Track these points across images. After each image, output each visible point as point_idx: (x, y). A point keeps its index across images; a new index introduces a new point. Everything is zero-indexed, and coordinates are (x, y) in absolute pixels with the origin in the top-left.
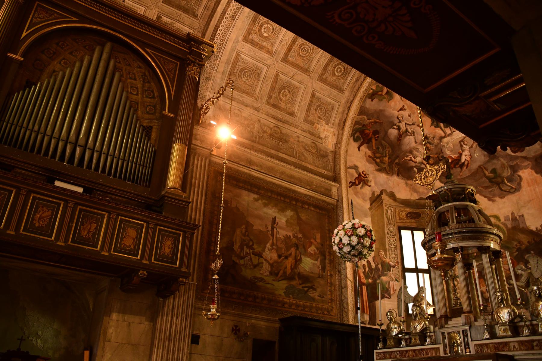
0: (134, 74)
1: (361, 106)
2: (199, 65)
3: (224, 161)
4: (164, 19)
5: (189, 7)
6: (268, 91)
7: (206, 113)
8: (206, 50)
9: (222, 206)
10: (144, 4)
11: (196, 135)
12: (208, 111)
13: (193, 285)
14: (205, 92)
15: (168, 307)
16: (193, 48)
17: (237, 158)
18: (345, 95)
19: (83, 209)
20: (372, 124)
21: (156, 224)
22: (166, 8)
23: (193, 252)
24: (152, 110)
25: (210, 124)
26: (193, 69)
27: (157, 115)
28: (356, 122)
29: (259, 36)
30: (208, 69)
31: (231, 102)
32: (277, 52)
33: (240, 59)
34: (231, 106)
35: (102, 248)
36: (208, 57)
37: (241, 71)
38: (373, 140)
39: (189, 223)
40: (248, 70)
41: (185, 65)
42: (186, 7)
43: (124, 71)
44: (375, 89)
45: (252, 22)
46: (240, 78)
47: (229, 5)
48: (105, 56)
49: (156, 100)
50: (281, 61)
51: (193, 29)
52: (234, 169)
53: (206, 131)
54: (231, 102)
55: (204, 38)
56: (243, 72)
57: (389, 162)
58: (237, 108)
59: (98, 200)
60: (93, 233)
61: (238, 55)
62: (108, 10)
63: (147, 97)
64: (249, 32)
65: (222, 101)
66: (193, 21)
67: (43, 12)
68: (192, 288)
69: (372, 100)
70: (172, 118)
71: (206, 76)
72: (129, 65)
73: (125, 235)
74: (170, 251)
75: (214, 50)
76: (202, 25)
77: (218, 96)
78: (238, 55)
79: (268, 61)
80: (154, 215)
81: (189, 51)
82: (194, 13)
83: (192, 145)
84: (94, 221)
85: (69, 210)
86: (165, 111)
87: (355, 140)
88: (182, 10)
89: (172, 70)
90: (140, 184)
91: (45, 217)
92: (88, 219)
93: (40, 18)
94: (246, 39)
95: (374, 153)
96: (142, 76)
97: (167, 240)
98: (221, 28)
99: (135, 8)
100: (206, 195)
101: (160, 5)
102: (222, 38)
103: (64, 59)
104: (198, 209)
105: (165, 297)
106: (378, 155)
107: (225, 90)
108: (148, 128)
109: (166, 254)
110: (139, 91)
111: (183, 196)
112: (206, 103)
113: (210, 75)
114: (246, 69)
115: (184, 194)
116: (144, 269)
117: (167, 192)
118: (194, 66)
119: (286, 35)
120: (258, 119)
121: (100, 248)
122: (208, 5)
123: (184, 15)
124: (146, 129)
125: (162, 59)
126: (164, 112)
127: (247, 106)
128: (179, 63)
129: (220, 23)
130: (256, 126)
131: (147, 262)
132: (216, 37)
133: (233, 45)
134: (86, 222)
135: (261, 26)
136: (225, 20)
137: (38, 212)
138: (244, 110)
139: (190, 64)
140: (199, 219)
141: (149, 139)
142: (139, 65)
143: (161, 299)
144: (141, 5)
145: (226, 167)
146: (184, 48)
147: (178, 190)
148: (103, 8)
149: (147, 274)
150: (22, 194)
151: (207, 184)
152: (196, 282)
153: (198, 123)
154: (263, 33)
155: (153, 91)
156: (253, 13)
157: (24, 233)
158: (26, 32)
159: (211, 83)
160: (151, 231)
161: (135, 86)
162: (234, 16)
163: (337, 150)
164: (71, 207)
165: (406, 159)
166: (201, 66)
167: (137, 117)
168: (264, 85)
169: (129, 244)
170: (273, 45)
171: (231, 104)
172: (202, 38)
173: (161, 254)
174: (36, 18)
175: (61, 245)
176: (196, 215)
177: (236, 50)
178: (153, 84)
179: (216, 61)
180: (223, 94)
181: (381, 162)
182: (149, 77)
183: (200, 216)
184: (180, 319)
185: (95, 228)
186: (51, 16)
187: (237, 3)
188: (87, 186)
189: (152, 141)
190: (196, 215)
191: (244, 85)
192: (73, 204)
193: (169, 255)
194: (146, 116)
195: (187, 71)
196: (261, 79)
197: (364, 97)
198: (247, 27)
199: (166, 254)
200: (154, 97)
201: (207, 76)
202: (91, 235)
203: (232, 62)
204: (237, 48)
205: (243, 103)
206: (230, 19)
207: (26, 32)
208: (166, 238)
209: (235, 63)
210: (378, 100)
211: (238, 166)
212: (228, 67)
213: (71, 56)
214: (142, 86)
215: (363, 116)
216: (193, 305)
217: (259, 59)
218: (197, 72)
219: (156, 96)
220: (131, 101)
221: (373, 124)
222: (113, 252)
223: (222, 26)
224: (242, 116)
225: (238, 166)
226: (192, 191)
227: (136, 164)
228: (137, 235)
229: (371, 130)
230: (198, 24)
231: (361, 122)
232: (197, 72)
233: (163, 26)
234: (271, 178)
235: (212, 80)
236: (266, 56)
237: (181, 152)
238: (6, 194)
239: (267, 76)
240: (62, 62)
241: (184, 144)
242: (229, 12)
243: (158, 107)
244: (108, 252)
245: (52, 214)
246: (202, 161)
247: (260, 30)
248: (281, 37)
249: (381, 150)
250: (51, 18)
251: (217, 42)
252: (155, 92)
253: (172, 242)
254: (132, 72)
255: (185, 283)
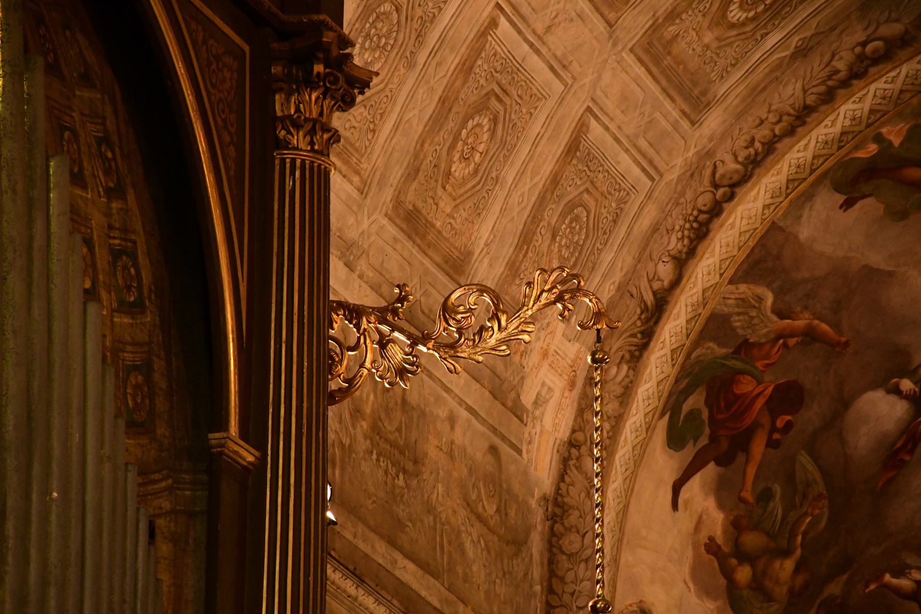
1: (774, 228)
18: (697, 134)
20: (785, 345)
28: (713, 317)
38: (758, 447)
44: (896, 142)
57: (791, 591)
69: (848, 204)
86: (225, 427)
87: (675, 440)
95: (736, 526)
106: (752, 540)
163: (575, 495)
165: (887, 586)
181: (758, 585)
197: (812, 171)
210: (881, 207)
215: (761, 290)
221: (792, 342)
229: (767, 378)
231: (737, 322)
249: (777, 507)
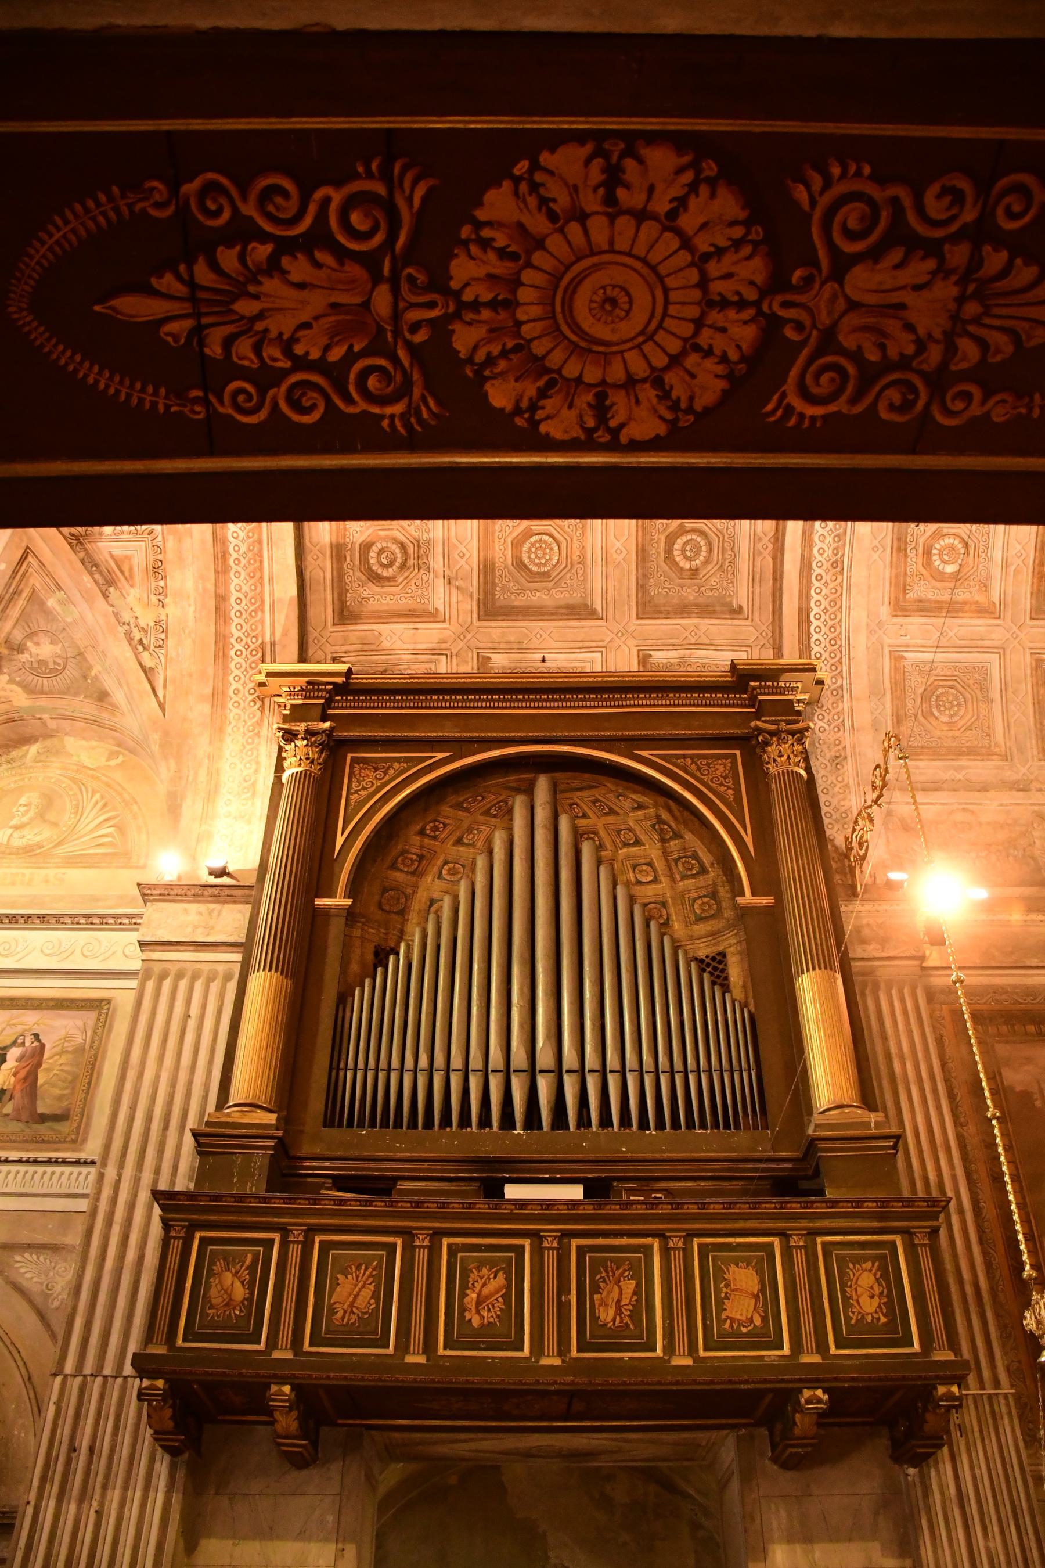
0: (630, 830)
2: (793, 733)
3: (954, 977)
4: (660, 657)
5: (709, 597)
6: (1032, 719)
7: (863, 858)
8: (799, 685)
9: (994, 1117)
10: (594, 644)
11: (858, 930)
12: (867, 847)
13: (1002, 1401)
14: (844, 799)
15: (942, 1493)
16: (760, 698)
17: (1012, 953)
19: (707, 1245)
21: (808, 1234)
22: (654, 628)
23: (969, 1289)
24: (710, 906)
25: (890, 885)
26: (780, 752)
27: (728, 913)
29: (934, 582)
30: (826, 733)
31: (913, 797)
32: (1009, 599)
33: (909, 668)
34: (917, 808)
35: (670, 1348)
36: (814, 702)
37: (925, 697)
39: (909, 1202)
40: (943, 687)
41: (758, 750)
42: (701, 600)
43: (602, 833)
45: (894, 554)
46: (932, 720)
47: (811, 540)
48: (542, 814)
49: (712, 874)
50: (1031, 618)
51: (744, 649)
52: (1015, 987)
53: (887, 907)
54: (913, 797)
55: (782, 657)
56: (933, 699)
58: (956, 806)
59: (621, 1209)
60: (631, 1307)
61: (897, 659)
62: (584, 700)
63: (684, 877)
64: (900, 585)
65: (899, 802)
66: (737, 628)
67: (368, 772)
68: (1004, 1409)
70: (767, 909)
71: (828, 756)
72: (612, 812)
73: (724, 1290)
74: (879, 1306)
75: (819, 675)
76: (764, 628)
77: (875, 796)
78: (897, 659)
79: (993, 636)
80: (794, 1205)
81: (753, 710)
82: (730, 604)
83: (852, 964)
84: (625, 1271)
85: (551, 1259)
88: (694, 615)
89: (725, 778)
90: (737, 1126)
91: (491, 1295)
92: (606, 1271)
93: (364, 789)
94: (900, 607)
96: (653, 826)
97: (857, 1274)
98: (815, 610)
99: (577, 665)
100: (952, 1097)
101: (633, 628)
102: (831, 636)
103: (446, 863)
104: (939, 1149)
105: (920, 1460)
107: (886, 771)
108: (713, 959)
109: (869, 1319)
110: (659, 869)
111: (869, 1123)
112: (854, 830)
113: (840, 747)
114: (937, 688)
115: (872, 1114)
116: (814, 1383)
117: (817, 1126)
118: (782, 741)
119: (1013, 541)
120: (1034, 812)
121: (791, 1348)
122: (758, 570)
123: (704, 623)
124: (708, 965)
125: (689, 761)
126: (740, 900)
127: (984, 788)
128: (738, 752)
129: (809, 598)
130: (1036, 834)
131: (816, 1359)
132: (813, 640)
133: (868, 638)
134: (604, 1281)
135: (928, 552)
136: (816, 584)
137: (470, 1285)
138: (980, 804)
139: (767, 744)
140: (954, 1177)
141: (726, 989)
142: (637, 802)
143: (912, 1471)
144: (589, 649)
145: (965, 994)
146: (737, 706)
147: (854, 1109)
148: (498, 700)
149: (826, 1397)
150: (420, 1247)
151: (943, 1065)
152: (1012, 1386)
153: (852, 893)
154: (941, 568)
155: (695, 856)
156: (886, 528)
157: (449, 1353)
158: (342, 833)
159: (850, 770)
160: (799, 1257)
161: (643, 861)
162: (836, 562)
164: (553, 1249)
166: (800, 735)
167: (673, 940)
168: (1012, 707)
169: (744, 1313)
170: (985, 587)
171: (915, 801)
172: (779, 658)
173: (853, 1322)
174: (356, 792)
175: (552, 1367)
176: (938, 1169)
177: (886, 650)
178: (688, 836)
179: (840, 704)
180: (884, 785)
182: (673, 824)
183: (952, 1166)
184: (996, 1529)
185: (635, 1293)
186: (386, 773)
187: (831, 524)
188: (590, 1176)
189: (737, 992)
190: (938, 1169)
191: (950, 734)
192: (556, 1237)
193: (879, 1319)
194: (701, 929)
195: (767, 763)
196: (996, 695)
198: (887, 575)
199: (869, 1319)
200: (703, 871)
201: (833, 754)
202: (629, 1316)
203: (888, 685)
204: (887, 641)
205: (969, 786)
206: (830, 574)
207: (342, 833)
208: (851, 1266)
209: (899, 685)
211: (1025, 975)
212: (883, 704)
213: (462, 849)
214: (660, 852)
216: (1027, 1469)
217: (963, 643)
218: (796, 756)
219: (707, 865)
220: (645, 905)
222: (706, 1349)
223: (818, 603)
224: (980, 824)
225: (1025, 975)
226: (903, 1097)
227: (709, 1072)
228: (762, 1281)
230: (751, 628)
232: (796, 756)
233: (661, 676)
234: (1039, 975)
235: (849, 758)
236: (978, 626)
237: (827, 996)
238: (382, 1256)
239: (1009, 678)
240: (444, 872)
241: (826, 968)
242: (819, 558)
243: (723, 892)
244: (690, 1354)
245: (508, 1279)
246: (902, 1000)
247: (928, 564)
248: (998, 555)
250: (387, 777)
251: (822, 652)
252: (700, 854)
253: (875, 1275)
254: (623, 827)
255: (960, 1398)
